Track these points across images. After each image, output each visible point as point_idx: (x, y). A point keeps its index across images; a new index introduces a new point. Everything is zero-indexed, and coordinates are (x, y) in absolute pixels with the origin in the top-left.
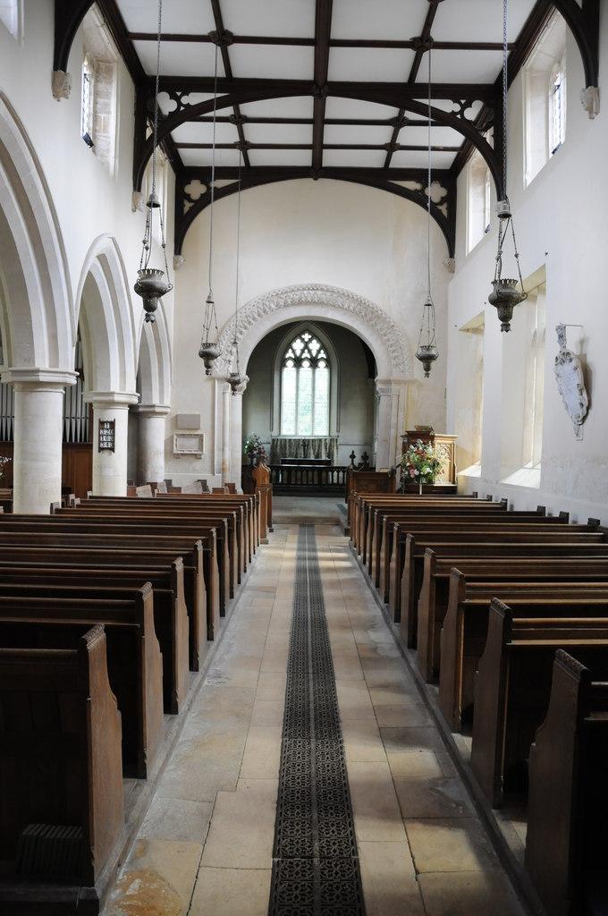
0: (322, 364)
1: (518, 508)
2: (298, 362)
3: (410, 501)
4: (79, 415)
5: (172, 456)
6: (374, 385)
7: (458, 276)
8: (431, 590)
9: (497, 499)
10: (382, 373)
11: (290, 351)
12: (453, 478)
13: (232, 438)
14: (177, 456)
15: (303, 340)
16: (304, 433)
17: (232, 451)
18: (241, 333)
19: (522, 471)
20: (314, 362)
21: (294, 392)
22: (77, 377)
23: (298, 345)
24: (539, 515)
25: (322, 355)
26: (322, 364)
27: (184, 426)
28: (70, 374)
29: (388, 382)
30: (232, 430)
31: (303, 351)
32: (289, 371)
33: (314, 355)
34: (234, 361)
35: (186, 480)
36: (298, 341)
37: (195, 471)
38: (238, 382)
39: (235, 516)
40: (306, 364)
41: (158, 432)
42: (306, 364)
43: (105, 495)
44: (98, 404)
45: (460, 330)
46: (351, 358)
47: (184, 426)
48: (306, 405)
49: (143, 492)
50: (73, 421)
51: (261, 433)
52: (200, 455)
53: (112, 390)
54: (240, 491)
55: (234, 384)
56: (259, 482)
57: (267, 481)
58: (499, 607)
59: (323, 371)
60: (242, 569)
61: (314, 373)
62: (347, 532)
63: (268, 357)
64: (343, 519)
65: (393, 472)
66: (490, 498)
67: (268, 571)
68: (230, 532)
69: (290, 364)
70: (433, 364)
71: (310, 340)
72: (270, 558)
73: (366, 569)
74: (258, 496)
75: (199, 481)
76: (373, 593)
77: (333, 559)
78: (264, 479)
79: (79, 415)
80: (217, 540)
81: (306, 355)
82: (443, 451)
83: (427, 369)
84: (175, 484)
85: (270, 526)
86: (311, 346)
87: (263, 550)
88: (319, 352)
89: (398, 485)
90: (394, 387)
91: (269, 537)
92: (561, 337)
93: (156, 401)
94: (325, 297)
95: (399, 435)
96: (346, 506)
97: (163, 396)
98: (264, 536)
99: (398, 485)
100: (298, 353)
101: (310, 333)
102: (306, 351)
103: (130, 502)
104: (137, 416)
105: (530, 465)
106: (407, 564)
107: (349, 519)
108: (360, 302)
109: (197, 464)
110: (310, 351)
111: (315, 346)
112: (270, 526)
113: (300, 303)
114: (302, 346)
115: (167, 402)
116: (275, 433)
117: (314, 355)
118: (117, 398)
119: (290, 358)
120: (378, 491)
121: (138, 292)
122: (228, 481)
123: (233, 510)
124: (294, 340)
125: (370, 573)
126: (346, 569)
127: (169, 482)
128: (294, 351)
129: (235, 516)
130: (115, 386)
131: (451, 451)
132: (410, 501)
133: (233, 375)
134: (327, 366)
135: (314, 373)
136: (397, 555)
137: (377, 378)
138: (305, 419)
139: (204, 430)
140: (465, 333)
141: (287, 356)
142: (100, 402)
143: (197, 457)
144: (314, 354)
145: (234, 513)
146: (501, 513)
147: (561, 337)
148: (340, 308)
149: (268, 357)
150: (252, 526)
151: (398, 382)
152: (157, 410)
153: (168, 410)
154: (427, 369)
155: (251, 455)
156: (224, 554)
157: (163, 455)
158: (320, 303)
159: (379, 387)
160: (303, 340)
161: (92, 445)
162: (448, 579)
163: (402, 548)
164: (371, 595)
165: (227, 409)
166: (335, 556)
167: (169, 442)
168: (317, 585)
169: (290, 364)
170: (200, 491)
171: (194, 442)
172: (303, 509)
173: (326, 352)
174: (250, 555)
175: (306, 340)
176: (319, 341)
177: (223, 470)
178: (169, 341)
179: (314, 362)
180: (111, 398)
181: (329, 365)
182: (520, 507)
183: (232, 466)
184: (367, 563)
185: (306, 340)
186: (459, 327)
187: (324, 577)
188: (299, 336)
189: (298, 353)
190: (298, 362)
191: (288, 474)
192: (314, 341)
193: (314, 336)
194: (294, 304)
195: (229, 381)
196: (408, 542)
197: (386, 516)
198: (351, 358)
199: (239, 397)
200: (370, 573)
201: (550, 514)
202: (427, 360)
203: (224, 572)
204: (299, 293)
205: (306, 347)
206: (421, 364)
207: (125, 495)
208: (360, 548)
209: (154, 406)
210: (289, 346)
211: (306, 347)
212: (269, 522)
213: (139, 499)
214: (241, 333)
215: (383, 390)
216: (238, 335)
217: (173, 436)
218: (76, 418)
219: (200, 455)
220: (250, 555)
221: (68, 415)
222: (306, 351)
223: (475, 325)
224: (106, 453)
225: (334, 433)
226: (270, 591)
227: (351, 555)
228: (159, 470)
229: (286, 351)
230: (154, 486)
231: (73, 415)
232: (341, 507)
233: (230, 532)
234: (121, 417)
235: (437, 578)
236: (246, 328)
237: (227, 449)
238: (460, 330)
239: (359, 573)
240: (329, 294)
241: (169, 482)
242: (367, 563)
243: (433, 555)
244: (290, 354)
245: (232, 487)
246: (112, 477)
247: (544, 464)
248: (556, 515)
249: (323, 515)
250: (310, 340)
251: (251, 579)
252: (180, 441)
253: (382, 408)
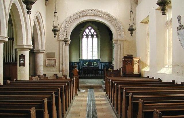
0: (95, 36)
1: (163, 81)
2: (87, 36)
3: (127, 79)
4: (13, 53)
5: (46, 66)
6: (112, 42)
7: (139, 5)
8: (125, 101)
9: (156, 78)
10: (115, 37)
11: (85, 32)
12: (140, 71)
13: (65, 60)
14: (47, 67)
15: (89, 29)
16: (90, 58)
17: (66, 65)
18: (68, 25)
19: (164, 68)
20: (92, 36)
21: (86, 56)
22: (8, 38)
23: (87, 31)
24: (173, 84)
25: (95, 33)
26: (95, 36)
27: (50, 56)
28: (6, 37)
29: (117, 41)
30: (66, 57)
31: (89, 33)
32: (84, 39)
33: (92, 34)
34: (67, 34)
35: (50, 74)
36: (87, 29)
37: (53, 71)
38: (67, 41)
39: (64, 87)
40: (90, 37)
41: (41, 59)
42: (90, 37)
43: (25, 80)
44: (19, 49)
45: (140, 23)
46: (104, 33)
47: (50, 56)
48: (90, 49)
49: (35, 79)
50: (7, 55)
51: (75, 60)
52: (55, 66)
53: (23, 44)
54: (68, 77)
55: (65, 41)
56: (75, 74)
57: (77, 74)
58: (157, 113)
59: (95, 39)
60: (68, 105)
61: (92, 39)
62: (105, 91)
63: (78, 33)
64: (103, 86)
65: (120, 70)
66: (148, 77)
67: (78, 106)
68: (62, 93)
69: (85, 37)
70: (134, 32)
71: (91, 29)
72: (78, 101)
73: (112, 104)
74: (74, 79)
75: (55, 74)
76: (116, 114)
77: (100, 100)
78: (76, 73)
79: (13, 53)
80: (61, 92)
81: (90, 34)
82: (136, 63)
83: (132, 34)
84: (47, 76)
85: (79, 89)
86: (91, 31)
87: (76, 98)
88: (94, 33)
89: (121, 74)
90: (119, 42)
91: (78, 93)
92: (179, 20)
93: (40, 48)
94: (95, 13)
95: (121, 58)
96: (104, 82)
97: (42, 46)
98: (76, 93)
99: (121, 74)
100: (87, 33)
101: (91, 27)
102: (90, 32)
103: (30, 82)
104: (33, 53)
105: (167, 66)
106: (124, 98)
107: (105, 86)
108: (107, 15)
109: (54, 69)
110: (91, 33)
111: (93, 31)
112: (79, 89)
113: (87, 15)
114: (88, 31)
115: (44, 49)
116: (81, 59)
117: (92, 34)
118: (25, 47)
119: (85, 35)
120: (115, 77)
121: (24, 3)
122: (64, 74)
123: (63, 84)
124: (86, 29)
125: (114, 106)
126: (105, 104)
127: (45, 75)
128: (86, 33)
129: (64, 87)
130: (24, 43)
131: (139, 63)
132: (127, 79)
133: (65, 39)
134: (97, 37)
135: (92, 39)
136: (125, 102)
137: (113, 39)
138: (90, 53)
139: (56, 58)
140: (142, 24)
141: (84, 34)
142: (20, 48)
143: (54, 66)
144: (92, 33)
145: (63, 86)
146: (159, 83)
147: (179, 20)
148: (100, 17)
149: (78, 33)
150: (71, 90)
151: (120, 40)
152: (40, 51)
153: (44, 51)
154: (132, 34)
155: (72, 66)
156: (66, 94)
157: (43, 66)
158: (94, 15)
159: (114, 42)
160: (89, 29)
161: (17, 63)
162: (138, 103)
163: (127, 98)
164: (114, 114)
165: (64, 50)
166: (101, 98)
167: (45, 61)
168: (95, 110)
169: (85, 37)
170: (55, 78)
171: (53, 62)
172: (89, 83)
173: (96, 33)
174: (73, 97)
175: (90, 29)
176: (94, 29)
177: (63, 71)
178: (44, 29)
179: (92, 36)
180: (23, 47)
181: (97, 37)
182: (164, 81)
183: (66, 69)
184: (110, 98)
185: (90, 29)
186: (140, 22)
187: (97, 107)
188: (87, 28)
189: (87, 33)
190: (87, 36)
191: (85, 71)
192: (92, 29)
193: (92, 28)
194: (85, 16)
195: (64, 41)
196: (130, 96)
197: (120, 86)
198: (104, 33)
199: (68, 47)
200: (114, 106)
201: (177, 83)
202: (131, 30)
203: (63, 103)
204: (86, 12)
205: (90, 31)
206: (129, 32)
207: (28, 79)
208: (109, 96)
209: (39, 50)
210: (84, 31)
211: (90, 31)
212: (78, 88)
213: (33, 81)
214: (68, 25)
215: (115, 43)
216: (67, 26)
217: (46, 60)
218: (12, 54)
219: (55, 66)
220: (73, 97)
221: (5, 53)
222: (90, 32)
223: (146, 20)
224: (22, 67)
225: (99, 58)
226: (77, 114)
227: (106, 99)
228: (42, 71)
229: (83, 33)
230: (39, 76)
231: (10, 53)
232: (102, 82)
233: (62, 93)
234: (27, 54)
235: (146, 113)
236: (69, 24)
237: (64, 64)
238: (140, 23)
239: (110, 105)
240: (97, 12)
241: (45, 75)
242: (110, 98)
243: (132, 95)
244: (85, 34)
245: (65, 76)
246: (24, 74)
247: (174, 66)
248: (180, 83)
249: (96, 85)
250: (91, 29)
251: (71, 109)
252: (48, 61)
253: (115, 50)
